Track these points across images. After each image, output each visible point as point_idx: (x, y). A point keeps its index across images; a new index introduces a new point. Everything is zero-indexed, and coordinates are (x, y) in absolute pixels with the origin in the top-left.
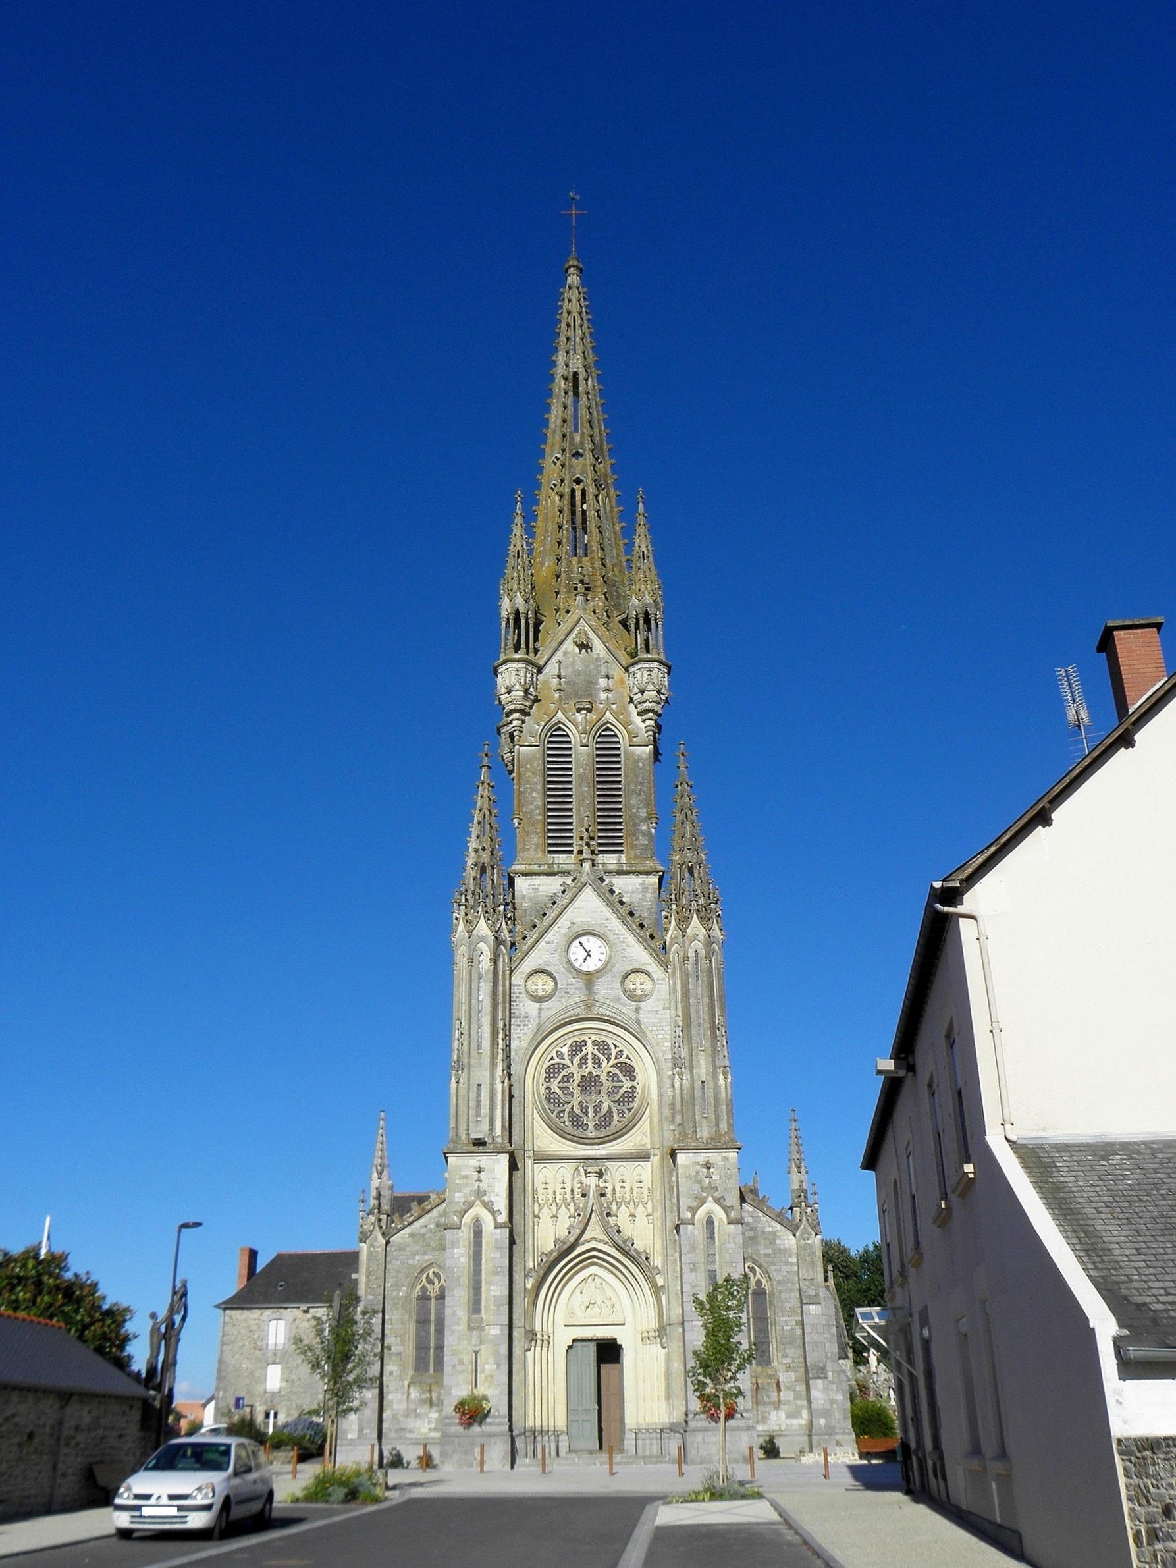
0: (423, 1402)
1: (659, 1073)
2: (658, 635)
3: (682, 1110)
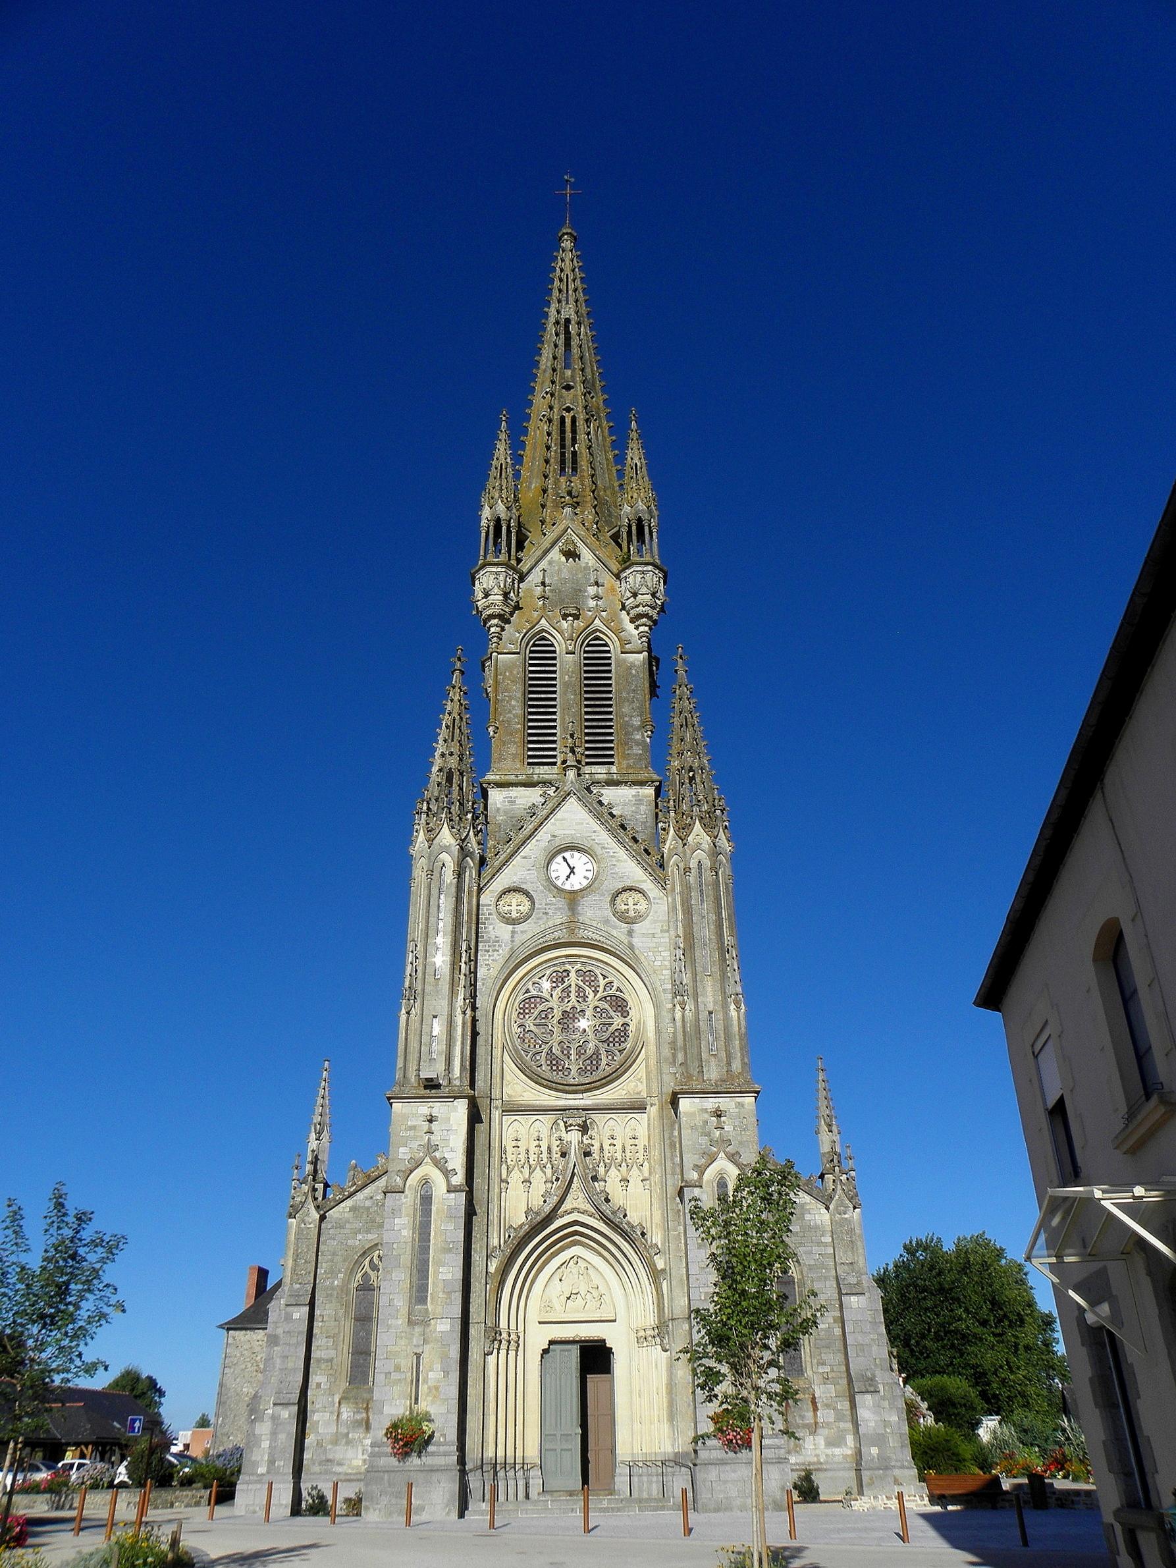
0: (357, 1424)
1: (657, 1005)
2: (654, 543)
3: (686, 1046)
